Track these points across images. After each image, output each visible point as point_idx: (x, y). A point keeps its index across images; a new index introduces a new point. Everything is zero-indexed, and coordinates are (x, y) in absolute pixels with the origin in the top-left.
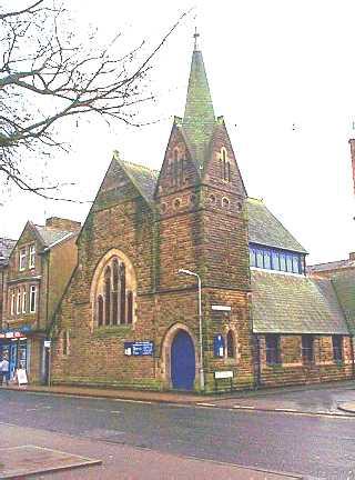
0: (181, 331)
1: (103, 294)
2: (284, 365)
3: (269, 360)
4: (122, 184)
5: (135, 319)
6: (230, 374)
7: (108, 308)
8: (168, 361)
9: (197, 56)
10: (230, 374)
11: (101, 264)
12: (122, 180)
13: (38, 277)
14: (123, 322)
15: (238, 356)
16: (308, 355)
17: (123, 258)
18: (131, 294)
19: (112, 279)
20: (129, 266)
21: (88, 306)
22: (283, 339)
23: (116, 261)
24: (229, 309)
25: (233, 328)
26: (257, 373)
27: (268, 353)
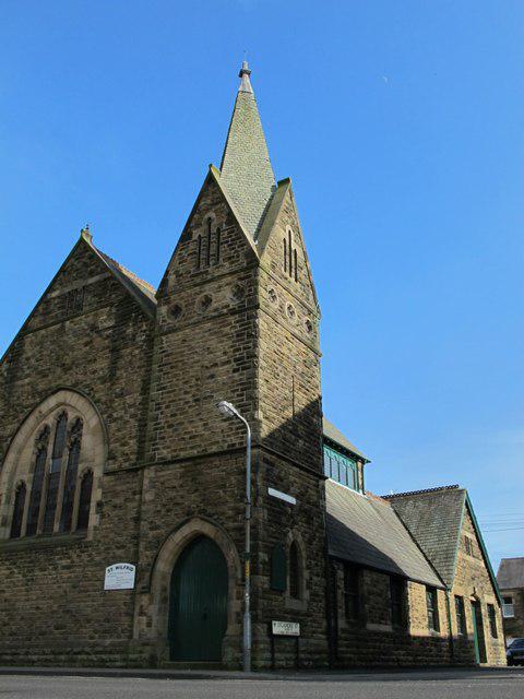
0: (199, 538)
1: (27, 477)
2: (371, 627)
5: (94, 519)
6: (295, 629)
8: (164, 600)
10: (295, 629)
11: (31, 421)
12: (92, 274)
14: (66, 526)
15: (306, 594)
18: (89, 474)
19: (50, 449)
20: (91, 420)
23: (63, 415)
25: (300, 539)
26: (331, 633)
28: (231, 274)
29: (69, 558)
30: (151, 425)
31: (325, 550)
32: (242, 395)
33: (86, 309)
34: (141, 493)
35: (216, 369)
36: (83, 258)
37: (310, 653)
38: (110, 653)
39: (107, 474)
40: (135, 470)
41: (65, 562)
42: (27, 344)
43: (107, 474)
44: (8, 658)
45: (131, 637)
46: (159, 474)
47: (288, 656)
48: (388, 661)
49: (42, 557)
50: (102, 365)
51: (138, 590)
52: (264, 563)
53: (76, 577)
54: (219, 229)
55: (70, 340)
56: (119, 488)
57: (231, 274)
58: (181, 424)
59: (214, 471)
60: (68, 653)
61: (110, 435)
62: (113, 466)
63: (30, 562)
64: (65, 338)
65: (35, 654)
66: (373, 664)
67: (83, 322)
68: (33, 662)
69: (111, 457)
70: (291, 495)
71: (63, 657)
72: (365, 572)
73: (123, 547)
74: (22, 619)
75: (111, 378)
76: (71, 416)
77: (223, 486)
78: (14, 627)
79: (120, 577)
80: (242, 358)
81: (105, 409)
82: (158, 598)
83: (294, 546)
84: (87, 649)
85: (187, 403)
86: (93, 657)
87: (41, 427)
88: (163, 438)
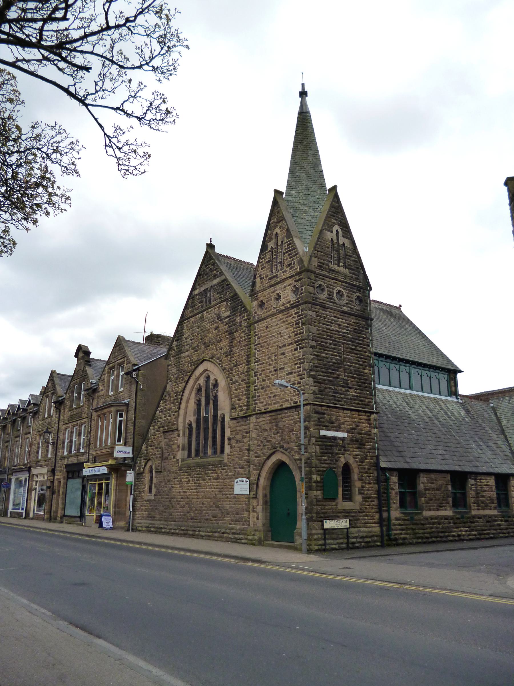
3: (403, 505)
4: (216, 282)
5: (227, 448)
6: (345, 524)
7: (198, 436)
9: (304, 121)
10: (345, 524)
13: (126, 401)
14: (215, 453)
15: (358, 498)
16: (460, 501)
17: (216, 374)
18: (223, 419)
20: (222, 383)
21: (176, 433)
22: (423, 479)
23: (208, 378)
24: (344, 435)
25: (351, 461)
27: (402, 495)
28: (291, 277)
29: (216, 473)
30: (252, 388)
31: (377, 464)
32: (300, 367)
33: (214, 303)
34: (250, 433)
35: (285, 348)
36: (211, 260)
37: (362, 537)
38: (239, 534)
39: (232, 419)
40: (246, 417)
41: (214, 476)
42: (185, 327)
43: (232, 419)
44: (191, 533)
45: (249, 525)
46: (259, 420)
47: (341, 541)
48: (449, 536)
49: (203, 471)
50: (225, 343)
51: (252, 496)
52: (317, 482)
53: (221, 485)
54: (282, 242)
55: (206, 325)
56: (238, 428)
57: (291, 277)
58: (268, 387)
59: (286, 420)
60: (219, 532)
61: (232, 393)
62: (235, 414)
63: (198, 474)
64: (204, 324)
65: (203, 532)
66: (430, 540)
67: (212, 313)
68: (203, 536)
69: (233, 408)
70: (343, 431)
71: (217, 535)
72: (421, 475)
73: (243, 468)
74: (196, 510)
75: (230, 354)
76: (212, 378)
77: (292, 431)
78: (192, 514)
79: (242, 487)
80: (299, 341)
81: (228, 373)
82: (261, 501)
83: (347, 468)
84: (228, 531)
85: (271, 372)
86: (231, 536)
87: (197, 386)
88: (259, 396)
